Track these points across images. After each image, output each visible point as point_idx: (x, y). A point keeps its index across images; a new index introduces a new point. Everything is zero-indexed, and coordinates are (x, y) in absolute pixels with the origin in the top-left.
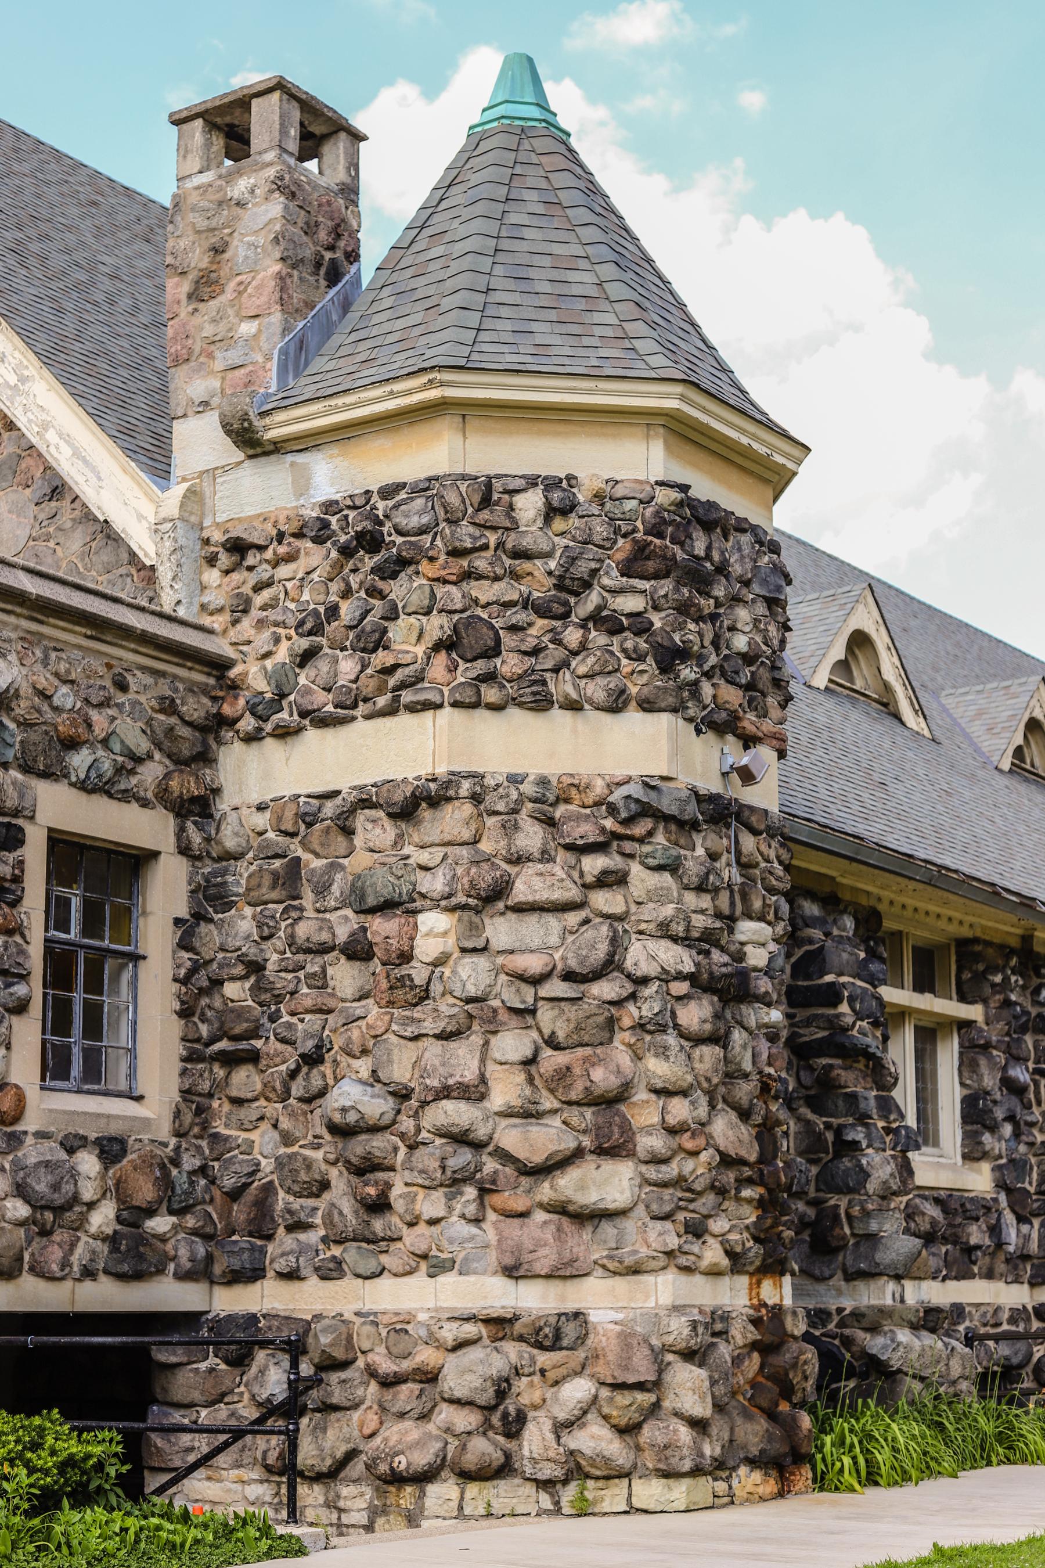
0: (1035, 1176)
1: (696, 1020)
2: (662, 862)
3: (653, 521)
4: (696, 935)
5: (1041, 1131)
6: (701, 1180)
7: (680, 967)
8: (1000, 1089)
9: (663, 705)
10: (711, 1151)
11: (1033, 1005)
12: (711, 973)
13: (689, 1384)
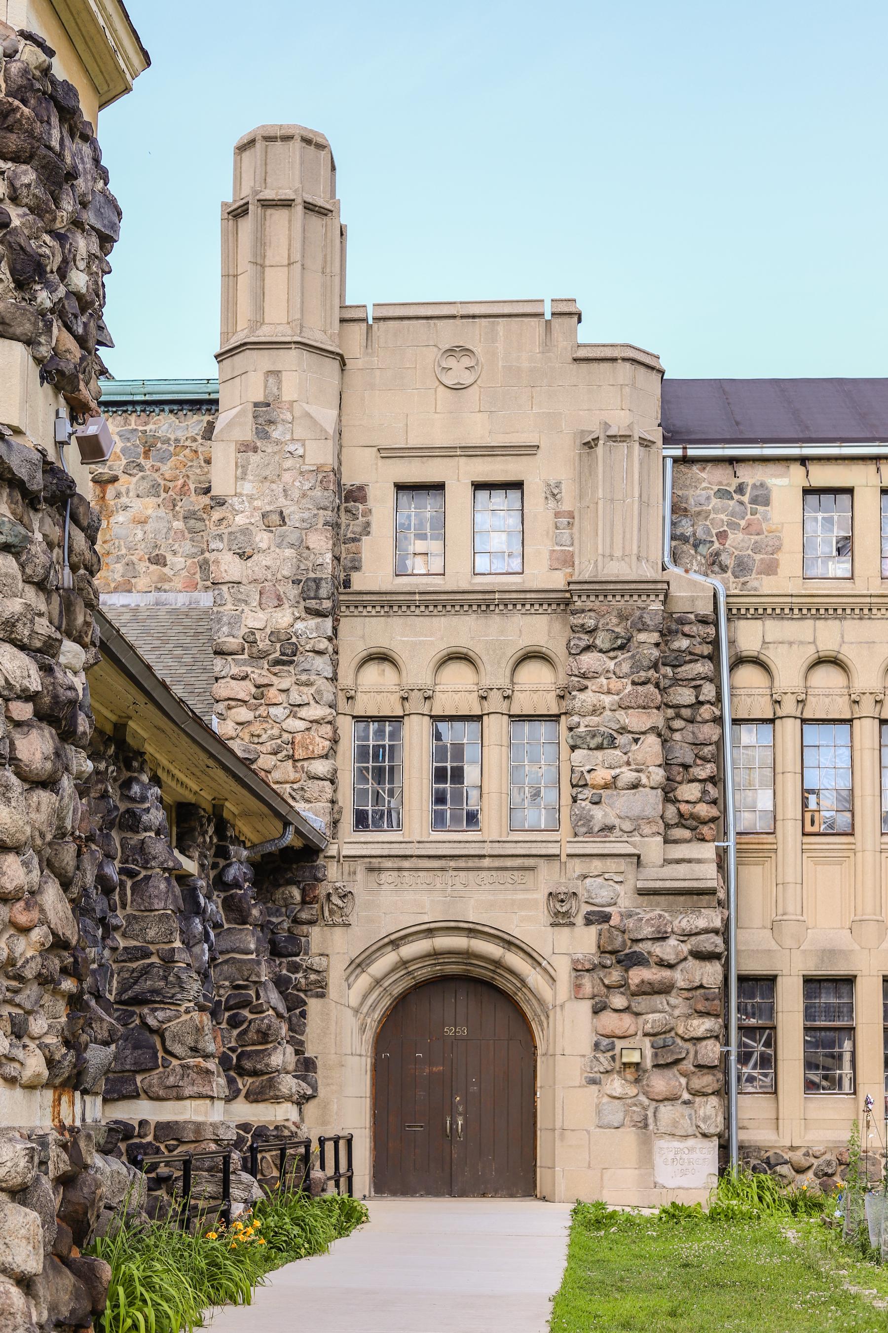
0: (115, 984)
1: (38, 756)
2: (10, 540)
3: (20, 81)
4: (38, 644)
5: (124, 935)
6: (32, 964)
7: (26, 682)
8: (96, 887)
9: (18, 331)
10: (45, 928)
11: (121, 800)
12: (55, 697)
13: (23, 1232)
